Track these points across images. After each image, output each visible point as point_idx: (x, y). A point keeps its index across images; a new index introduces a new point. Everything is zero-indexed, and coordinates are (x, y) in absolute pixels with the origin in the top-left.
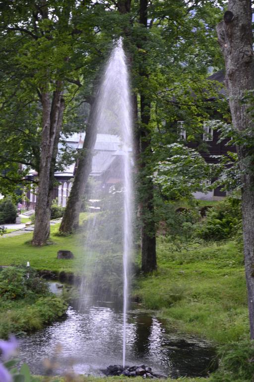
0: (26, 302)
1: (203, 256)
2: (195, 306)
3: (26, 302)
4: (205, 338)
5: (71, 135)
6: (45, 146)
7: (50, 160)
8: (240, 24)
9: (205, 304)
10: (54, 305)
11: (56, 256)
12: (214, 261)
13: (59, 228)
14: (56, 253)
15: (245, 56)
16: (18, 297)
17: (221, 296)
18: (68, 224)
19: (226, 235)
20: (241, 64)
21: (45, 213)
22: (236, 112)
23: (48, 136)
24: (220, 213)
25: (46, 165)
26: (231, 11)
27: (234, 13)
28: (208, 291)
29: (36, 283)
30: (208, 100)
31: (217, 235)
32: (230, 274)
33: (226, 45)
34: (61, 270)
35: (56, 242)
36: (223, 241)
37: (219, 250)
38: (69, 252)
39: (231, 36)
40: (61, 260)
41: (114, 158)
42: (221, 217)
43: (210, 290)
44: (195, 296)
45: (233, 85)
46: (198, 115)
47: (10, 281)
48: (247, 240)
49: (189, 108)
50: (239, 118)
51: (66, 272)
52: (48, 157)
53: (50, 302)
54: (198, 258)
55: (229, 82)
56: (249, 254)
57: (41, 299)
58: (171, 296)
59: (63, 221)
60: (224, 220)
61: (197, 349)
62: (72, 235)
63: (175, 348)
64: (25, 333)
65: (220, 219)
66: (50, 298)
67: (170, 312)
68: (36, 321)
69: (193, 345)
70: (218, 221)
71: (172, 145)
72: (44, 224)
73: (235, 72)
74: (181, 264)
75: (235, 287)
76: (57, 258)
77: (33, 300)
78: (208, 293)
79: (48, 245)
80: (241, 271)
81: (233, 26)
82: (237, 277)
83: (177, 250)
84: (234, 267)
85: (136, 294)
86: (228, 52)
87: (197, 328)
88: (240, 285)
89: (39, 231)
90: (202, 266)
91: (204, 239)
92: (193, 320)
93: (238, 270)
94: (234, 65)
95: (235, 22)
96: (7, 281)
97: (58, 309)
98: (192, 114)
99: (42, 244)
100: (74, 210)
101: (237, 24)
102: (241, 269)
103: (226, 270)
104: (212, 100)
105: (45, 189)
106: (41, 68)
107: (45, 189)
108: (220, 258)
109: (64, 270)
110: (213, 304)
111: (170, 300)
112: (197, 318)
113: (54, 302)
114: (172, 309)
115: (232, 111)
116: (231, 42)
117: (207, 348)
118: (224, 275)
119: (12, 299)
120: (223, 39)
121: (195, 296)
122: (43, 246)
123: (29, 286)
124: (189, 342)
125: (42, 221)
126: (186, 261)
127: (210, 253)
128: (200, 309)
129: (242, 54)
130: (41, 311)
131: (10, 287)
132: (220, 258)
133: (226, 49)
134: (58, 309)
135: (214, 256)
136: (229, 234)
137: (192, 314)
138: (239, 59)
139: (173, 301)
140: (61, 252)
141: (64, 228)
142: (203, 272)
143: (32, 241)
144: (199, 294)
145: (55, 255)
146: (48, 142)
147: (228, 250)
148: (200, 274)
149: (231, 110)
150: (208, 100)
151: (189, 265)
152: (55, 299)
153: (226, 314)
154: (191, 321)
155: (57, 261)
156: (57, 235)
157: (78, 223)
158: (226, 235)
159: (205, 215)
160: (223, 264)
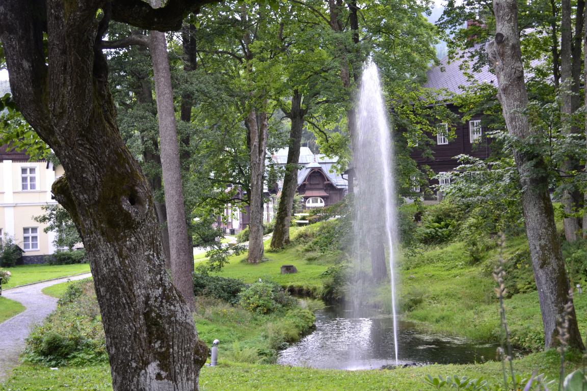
0: (277, 315)
1: (428, 260)
2: (437, 307)
3: (277, 315)
4: (457, 335)
5: (276, 151)
6: (255, 164)
7: (260, 177)
8: (511, 44)
9: (446, 304)
10: (304, 317)
11: (280, 272)
12: (440, 264)
13: (270, 244)
14: (280, 269)
15: (517, 72)
16: (268, 311)
17: (460, 296)
18: (279, 239)
19: (446, 238)
20: (514, 79)
21: (258, 230)
22: (511, 122)
23: (258, 155)
24: (438, 217)
25: (257, 183)
26: (501, 32)
27: (504, 34)
28: (445, 292)
29: (281, 297)
30: (426, 108)
31: (438, 238)
32: (461, 275)
33: (497, 63)
34: (289, 285)
35: (270, 259)
36: (444, 244)
37: (443, 253)
38: (292, 266)
39: (502, 55)
40: (286, 275)
41: (309, 170)
42: (439, 220)
43: (447, 291)
44: (434, 298)
45: (507, 98)
46: (417, 123)
47: (260, 297)
48: (532, 236)
49: (408, 117)
50: (514, 127)
51: (294, 286)
52: (259, 175)
53: (300, 314)
54: (423, 262)
55: (503, 96)
56: (535, 248)
57: (290, 311)
58: (411, 300)
59: (274, 237)
60: (443, 223)
61: (454, 346)
62: (284, 250)
63: (434, 346)
64: (288, 344)
65: (439, 222)
66: (298, 310)
67: (414, 315)
68: (294, 332)
69: (449, 343)
70: (437, 224)
71: (459, 156)
72: (258, 241)
73: (509, 87)
74: (408, 269)
75: (470, 286)
76: (281, 273)
77: (282, 313)
78: (447, 294)
79: (263, 262)
80: (470, 271)
81: (503, 47)
82: (469, 277)
83: (412, 255)
84: (462, 268)
85: (373, 301)
86: (500, 69)
87: (445, 327)
88: (475, 285)
89: (254, 248)
90: (430, 269)
91: (424, 243)
92: (439, 321)
93: (467, 271)
94: (506, 80)
95: (506, 42)
96: (257, 297)
97: (308, 320)
98: (412, 122)
99: (258, 261)
100: (284, 226)
101: (508, 44)
102: (470, 270)
103: (454, 272)
104: (430, 108)
105: (257, 206)
106: (580, 118)
107: (257, 206)
108: (446, 261)
109: (292, 284)
110: (454, 304)
111: (411, 303)
112: (443, 318)
113: (304, 314)
114: (415, 312)
115: (507, 122)
116: (503, 60)
117: (464, 345)
118: (455, 276)
119: (265, 313)
120: (495, 58)
121: (434, 298)
122: (259, 263)
123: (276, 299)
124: (444, 341)
125: (256, 239)
126: (412, 266)
127: (435, 256)
128: (443, 310)
129: (514, 70)
130: (294, 322)
131: (261, 302)
132: (446, 261)
133: (497, 66)
134: (308, 320)
135: (439, 259)
136: (449, 236)
137: (437, 315)
138: (511, 74)
139: (414, 305)
140: (284, 267)
141: (276, 244)
142: (433, 275)
143: (247, 259)
144: (438, 296)
145: (279, 270)
146: (258, 159)
147: (452, 253)
148: (431, 277)
149: (506, 121)
150: (426, 108)
151: (417, 270)
152: (303, 311)
153: (471, 312)
154: (437, 321)
155: (282, 276)
156: (269, 251)
157: (289, 238)
158: (446, 238)
159: (420, 220)
160: (450, 266)
